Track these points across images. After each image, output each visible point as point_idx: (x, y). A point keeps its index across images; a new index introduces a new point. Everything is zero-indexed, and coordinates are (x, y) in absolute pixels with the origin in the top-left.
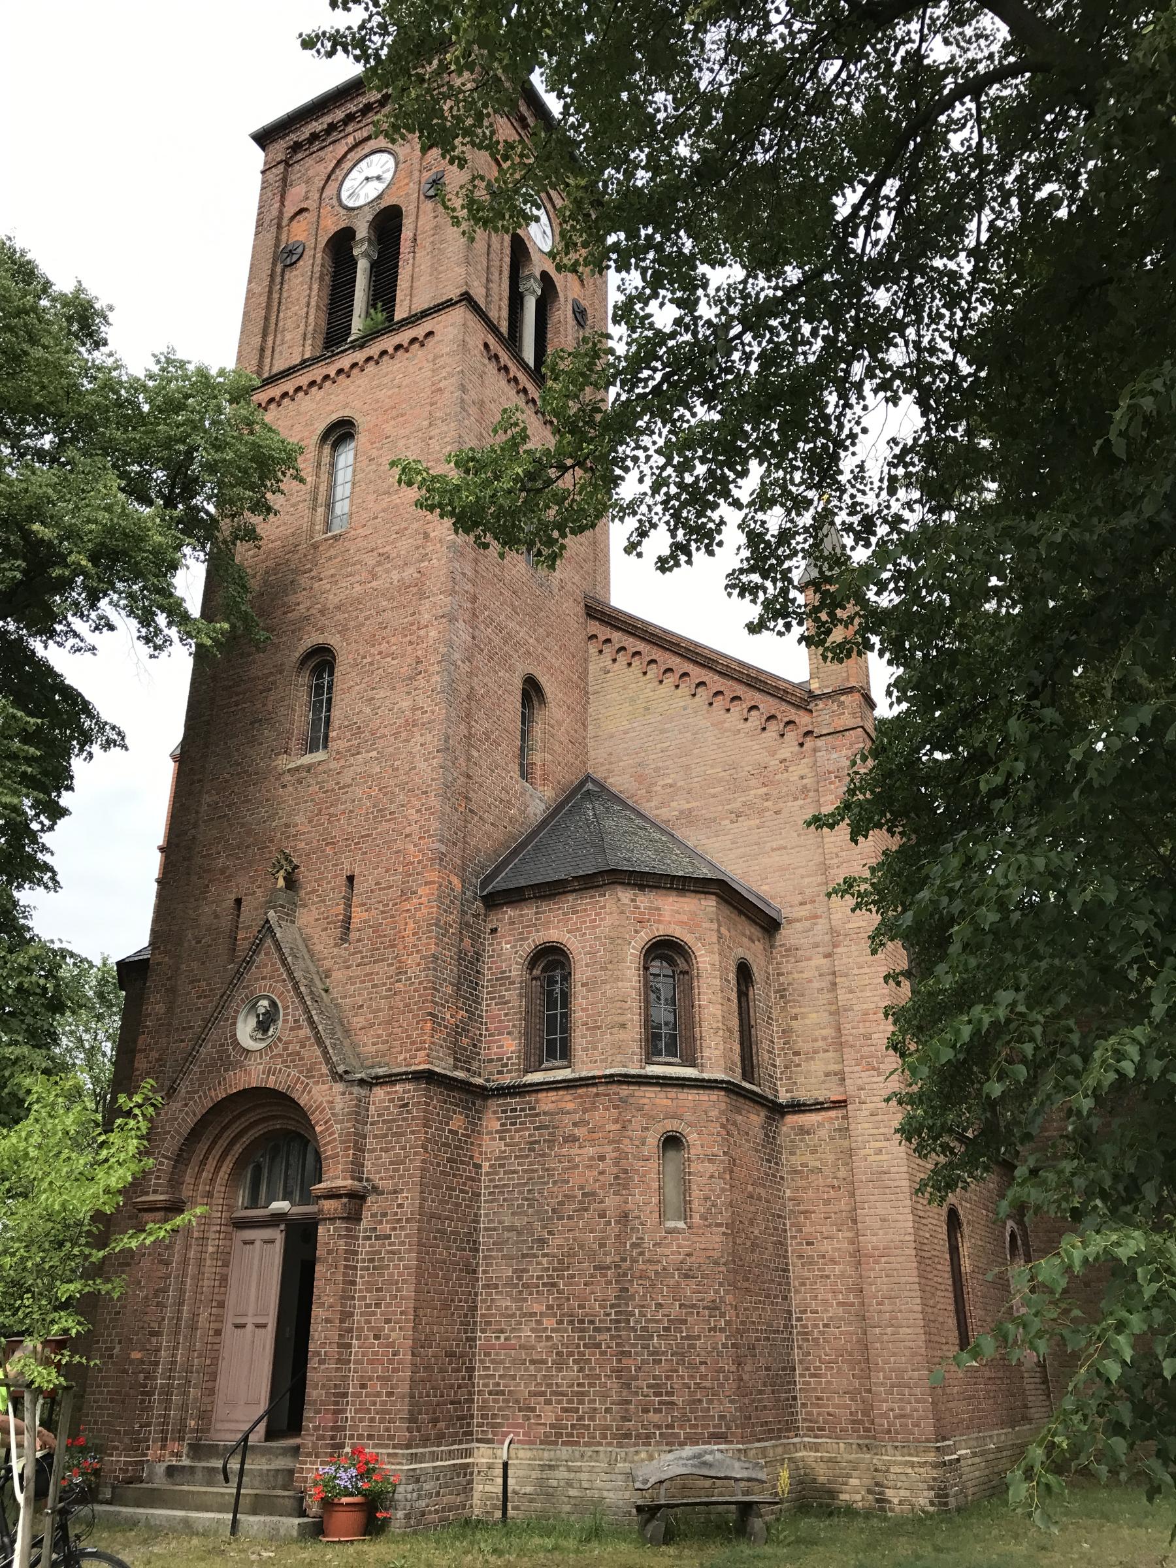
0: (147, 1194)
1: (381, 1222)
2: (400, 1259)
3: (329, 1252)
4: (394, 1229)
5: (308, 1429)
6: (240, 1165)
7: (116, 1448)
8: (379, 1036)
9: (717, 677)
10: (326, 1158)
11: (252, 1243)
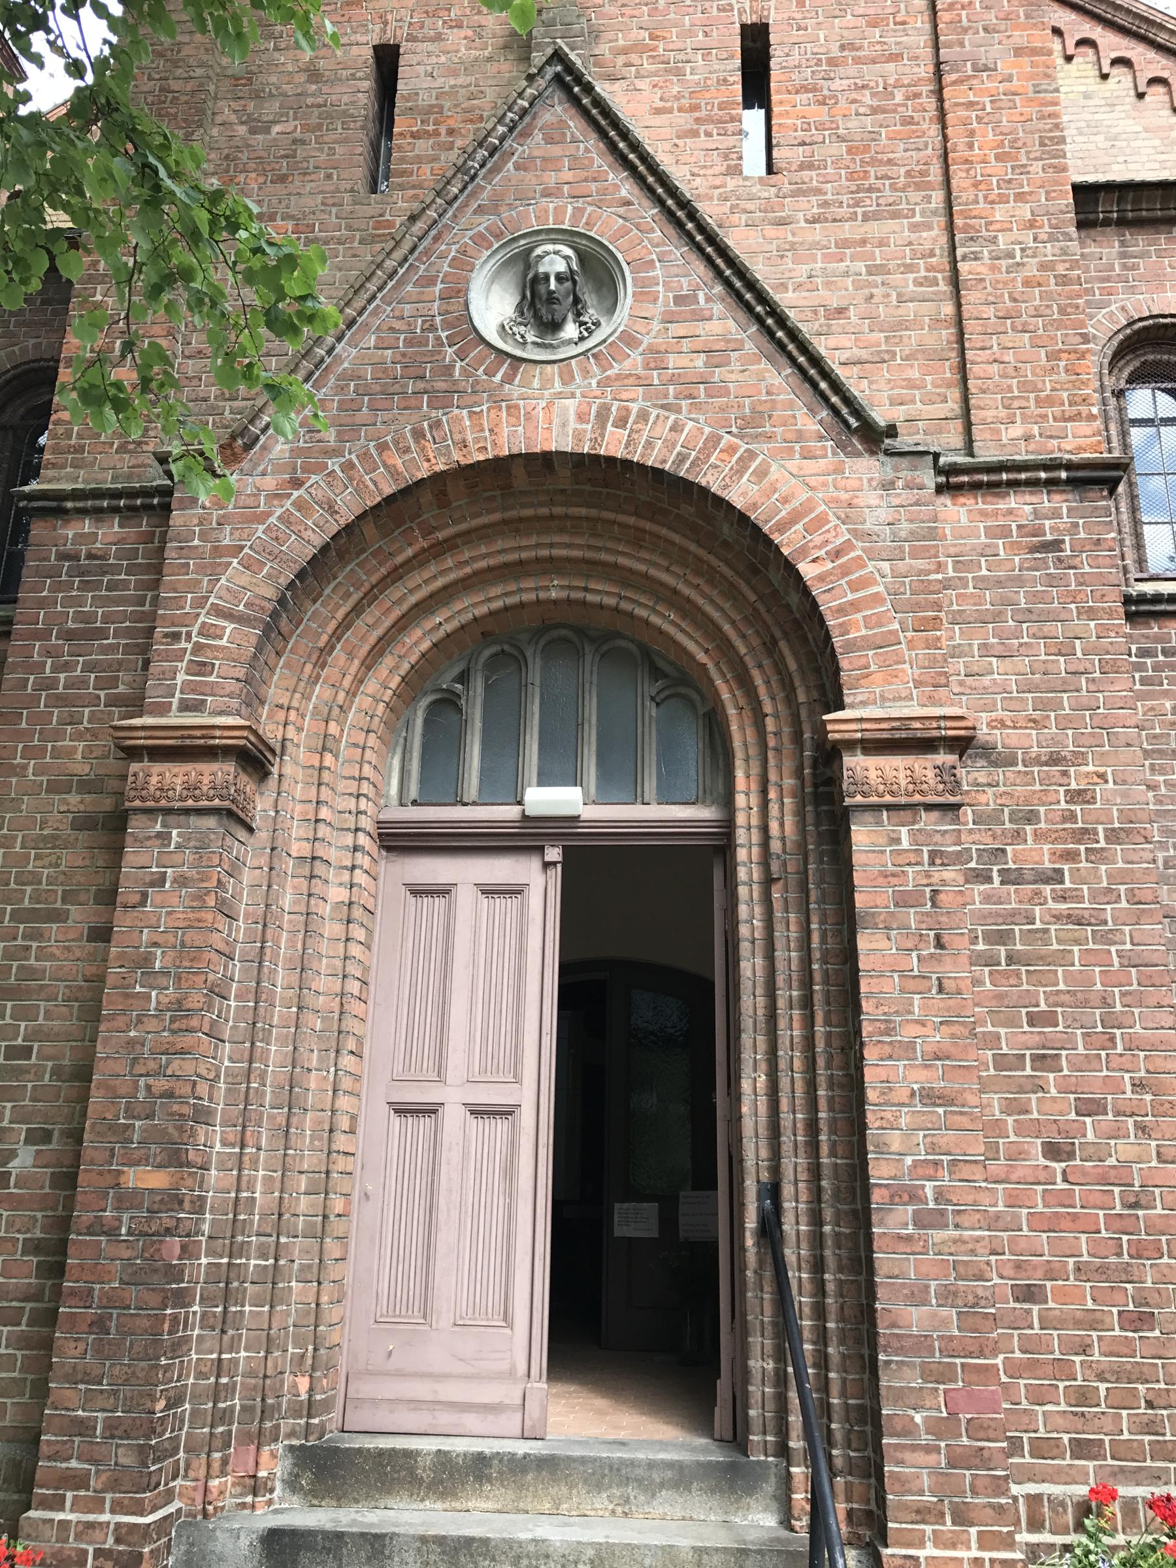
0: (164, 709)
1: (1018, 836)
2: (1106, 938)
3: (903, 900)
4: (1071, 856)
5: (909, 1430)
6: (412, 685)
7: (79, 1481)
8: (911, 385)
9: (1152, 54)
10: (851, 646)
11: (443, 891)
